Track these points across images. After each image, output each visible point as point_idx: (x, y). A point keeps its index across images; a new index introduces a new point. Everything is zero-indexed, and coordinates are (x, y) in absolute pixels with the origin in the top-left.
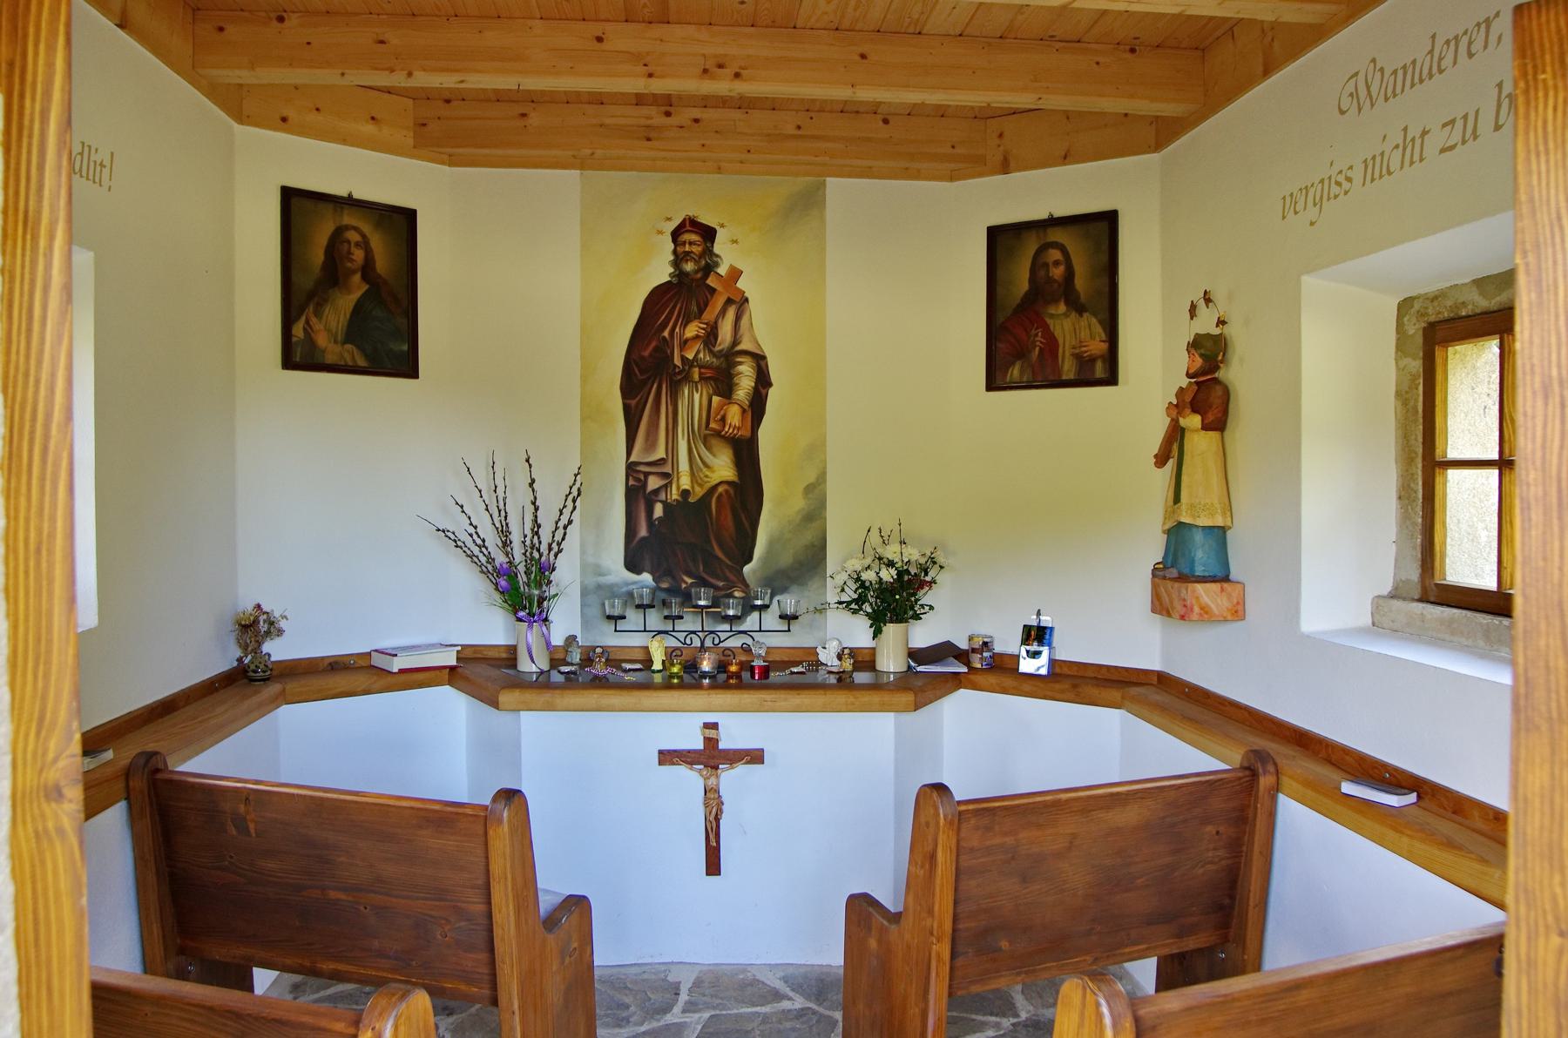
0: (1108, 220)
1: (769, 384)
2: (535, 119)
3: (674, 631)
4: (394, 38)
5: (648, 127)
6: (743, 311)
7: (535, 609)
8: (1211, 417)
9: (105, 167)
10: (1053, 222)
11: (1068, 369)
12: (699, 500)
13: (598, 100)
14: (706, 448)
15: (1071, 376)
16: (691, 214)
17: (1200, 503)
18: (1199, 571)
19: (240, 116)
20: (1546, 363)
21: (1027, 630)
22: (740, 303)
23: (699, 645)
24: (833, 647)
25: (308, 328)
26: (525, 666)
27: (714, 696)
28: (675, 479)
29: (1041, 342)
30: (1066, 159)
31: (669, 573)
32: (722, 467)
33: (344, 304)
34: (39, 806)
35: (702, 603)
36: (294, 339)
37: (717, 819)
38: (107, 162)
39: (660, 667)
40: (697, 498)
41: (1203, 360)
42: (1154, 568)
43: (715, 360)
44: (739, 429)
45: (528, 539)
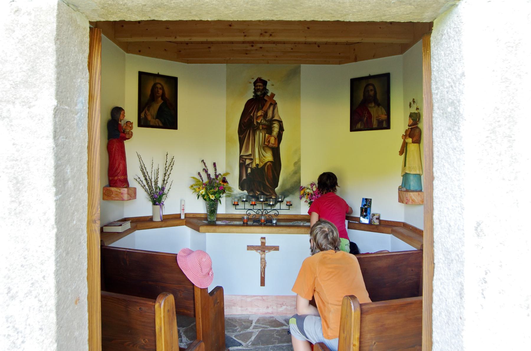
0: (387, 76)
1: (283, 130)
2: (213, 49)
3: (253, 209)
6: (275, 107)
8: (415, 139)
10: (370, 77)
11: (375, 124)
12: (262, 167)
14: (263, 150)
17: (412, 167)
18: (412, 188)
19: (128, 51)
20: (429, 122)
22: (274, 104)
23: (261, 214)
28: (254, 160)
32: (269, 157)
33: (156, 107)
34: (91, 224)
35: (262, 200)
36: (142, 118)
37: (264, 268)
40: (261, 166)
43: (266, 123)
44: (274, 144)
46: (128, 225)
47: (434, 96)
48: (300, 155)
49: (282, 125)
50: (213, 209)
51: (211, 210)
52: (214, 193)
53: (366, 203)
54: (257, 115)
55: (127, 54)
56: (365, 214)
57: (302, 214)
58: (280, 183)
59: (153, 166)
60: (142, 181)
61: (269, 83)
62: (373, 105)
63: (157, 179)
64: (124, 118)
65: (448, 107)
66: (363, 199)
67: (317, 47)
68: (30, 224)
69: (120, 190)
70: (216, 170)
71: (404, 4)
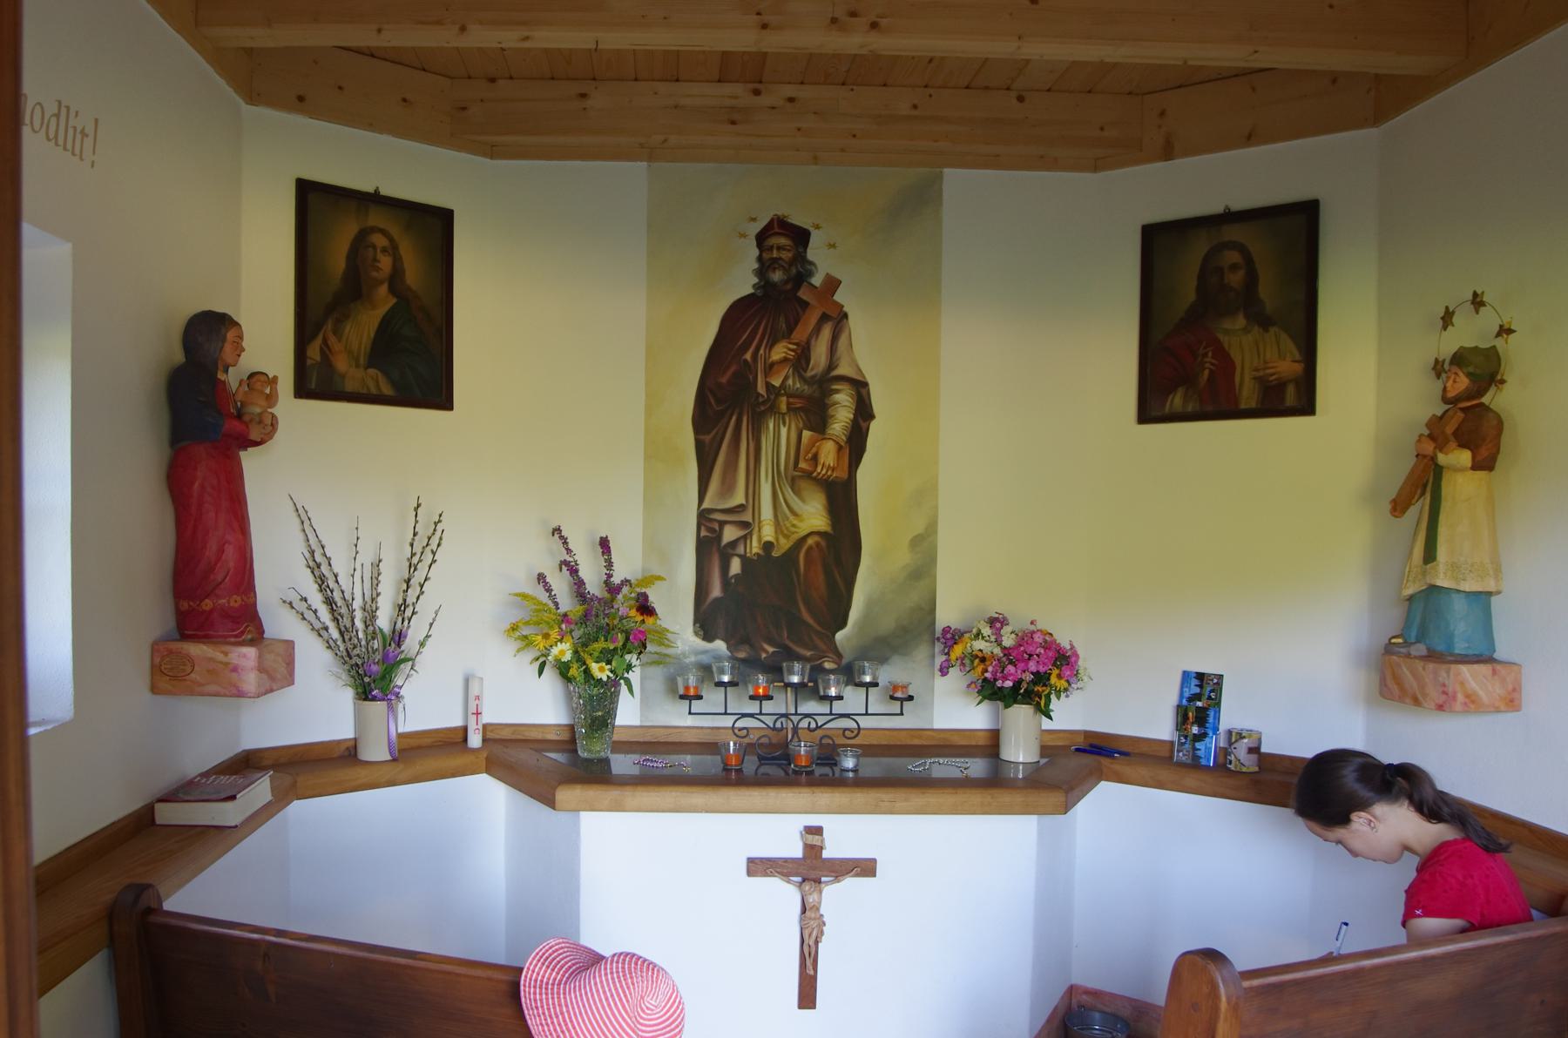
1: (871, 417)
3: (761, 714)
5: (732, 108)
9: (87, 136)
10: (1229, 217)
11: (1248, 394)
12: (784, 555)
14: (792, 490)
15: (1253, 405)
16: (779, 213)
18: (1460, 647)
22: (839, 319)
25: (325, 349)
27: (820, 795)
28: (756, 529)
29: (1212, 364)
30: (1250, 139)
32: (813, 515)
33: (363, 326)
35: (795, 679)
36: (309, 362)
38: (90, 129)
40: (783, 551)
41: (1470, 380)
42: (1390, 643)
43: (806, 387)
46: (261, 790)
48: (936, 507)
49: (866, 398)
50: (602, 716)
51: (594, 720)
52: (607, 657)
53: (1197, 690)
54: (769, 357)
55: (247, 109)
56: (1195, 730)
57: (937, 726)
58: (854, 614)
59: (357, 553)
60: (315, 612)
61: (816, 239)
62: (1241, 321)
63: (373, 600)
64: (239, 356)
66: (1186, 675)
67: (1015, 101)
69: (226, 654)
70: (609, 564)
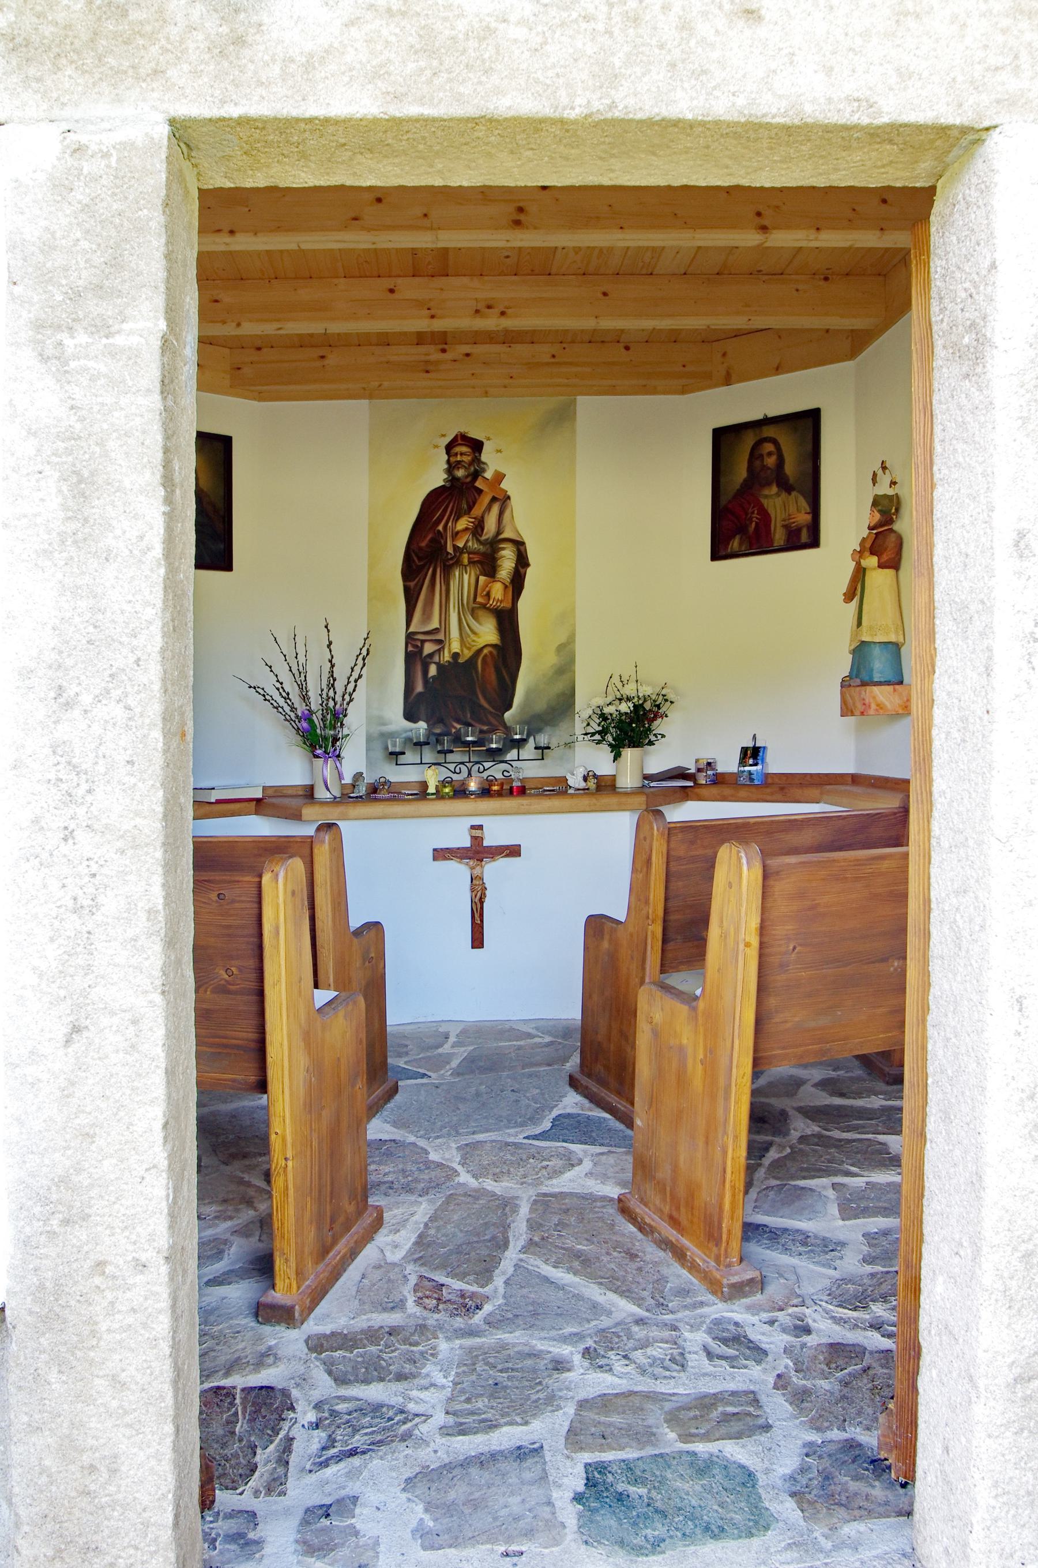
2: (332, 360)
4: (227, 298)
7: (330, 749)
8: (885, 558)
10: (767, 421)
11: (779, 536)
12: (466, 661)
13: (385, 340)
21: (744, 751)
22: (503, 500)
24: (581, 772)
26: (321, 794)
30: (778, 370)
31: (441, 721)
32: (487, 633)
37: (482, 903)
39: (434, 791)
44: (501, 602)
45: (324, 693)
47: (935, 328)
65: (964, 337)
67: (623, 350)
68: (107, 560)
71: (879, 140)
